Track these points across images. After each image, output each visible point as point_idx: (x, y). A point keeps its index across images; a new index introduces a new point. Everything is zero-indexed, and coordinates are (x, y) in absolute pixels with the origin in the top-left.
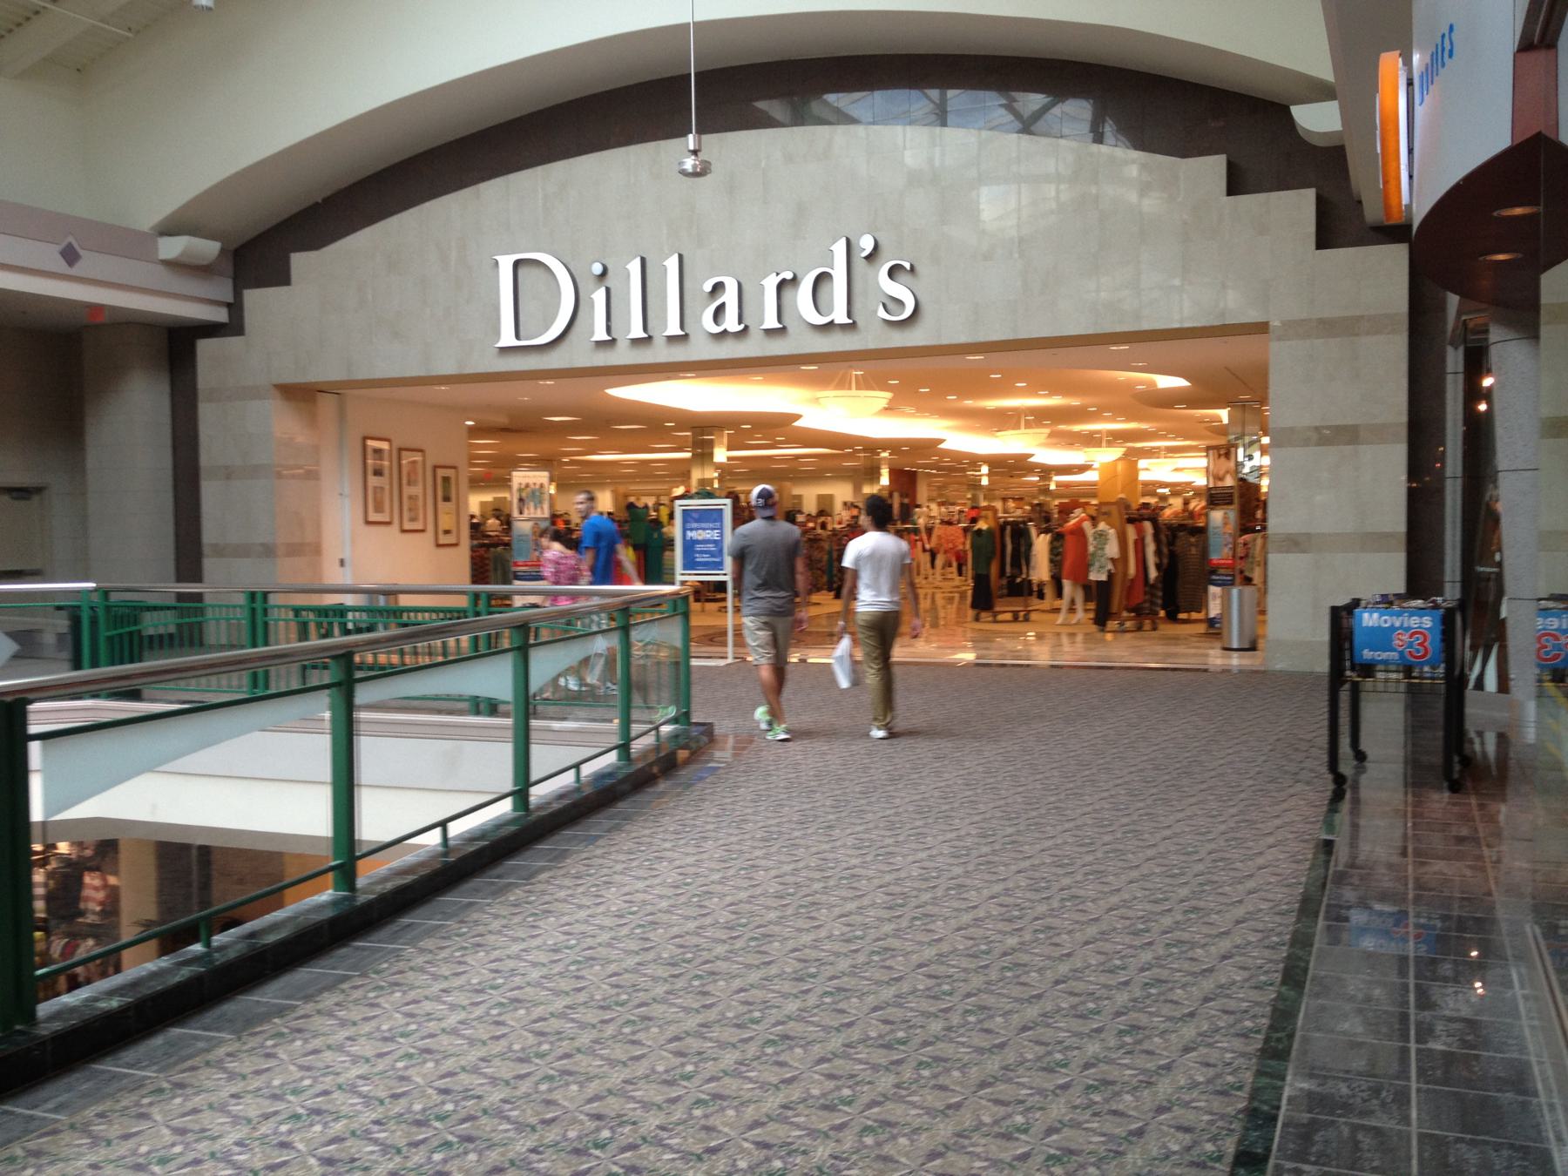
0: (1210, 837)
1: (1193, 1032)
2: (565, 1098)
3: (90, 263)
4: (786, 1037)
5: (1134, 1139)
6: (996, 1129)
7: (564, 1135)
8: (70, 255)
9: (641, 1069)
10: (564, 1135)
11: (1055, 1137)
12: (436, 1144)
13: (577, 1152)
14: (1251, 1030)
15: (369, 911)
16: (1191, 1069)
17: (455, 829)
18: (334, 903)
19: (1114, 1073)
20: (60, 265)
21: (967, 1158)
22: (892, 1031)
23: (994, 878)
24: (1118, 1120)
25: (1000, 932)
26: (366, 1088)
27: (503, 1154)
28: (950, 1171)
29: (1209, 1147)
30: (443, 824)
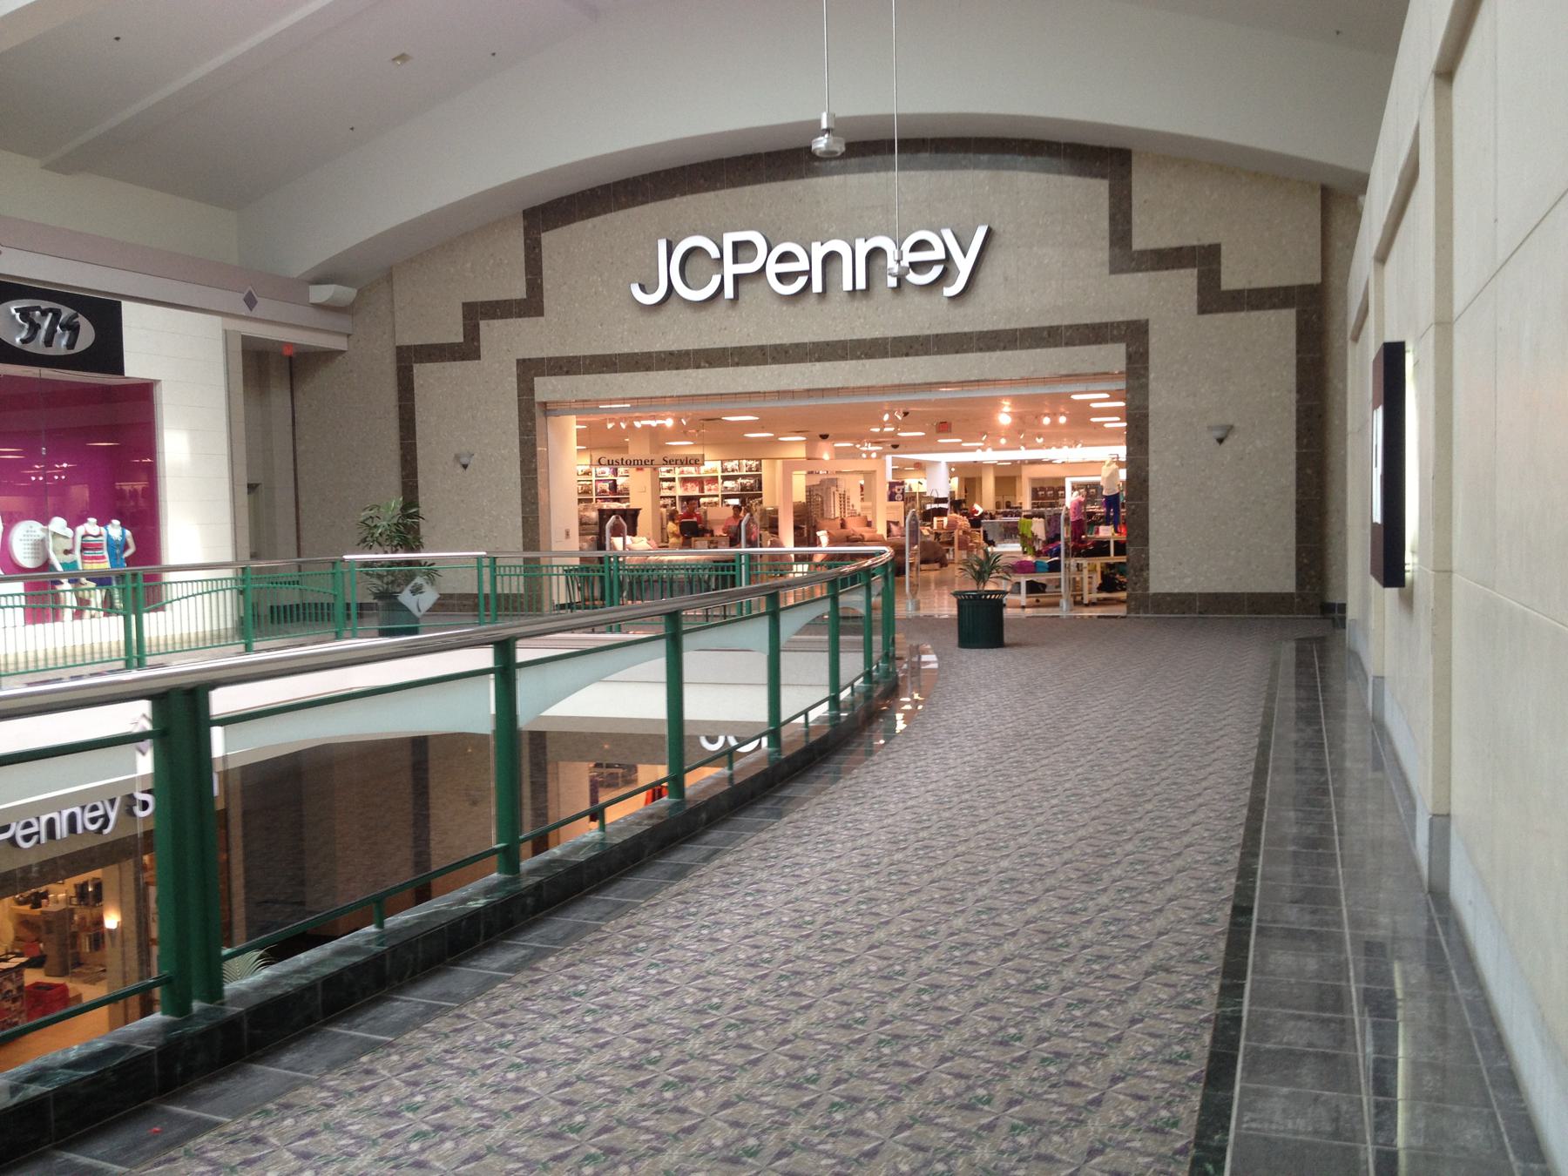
0: (1137, 816)
1: (1131, 1005)
2: (534, 1085)
3: (264, 307)
4: (745, 1021)
5: (984, 1134)
6: (958, 1101)
7: (457, 1144)
8: (250, 301)
9: (561, 1074)
10: (457, 1144)
11: (867, 1147)
12: (409, 1134)
13: (554, 1136)
14: (1192, 1002)
15: (712, 809)
16: (1138, 1042)
17: (813, 715)
18: (671, 808)
19: (1066, 1045)
20: (244, 310)
21: (815, 1156)
22: (849, 1012)
23: (967, 857)
24: (1077, 1090)
25: (809, 959)
26: (324, 1094)
27: (518, 1123)
28: (799, 1170)
29: (1164, 1113)
30: (805, 713)
